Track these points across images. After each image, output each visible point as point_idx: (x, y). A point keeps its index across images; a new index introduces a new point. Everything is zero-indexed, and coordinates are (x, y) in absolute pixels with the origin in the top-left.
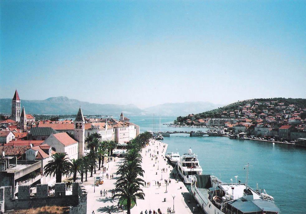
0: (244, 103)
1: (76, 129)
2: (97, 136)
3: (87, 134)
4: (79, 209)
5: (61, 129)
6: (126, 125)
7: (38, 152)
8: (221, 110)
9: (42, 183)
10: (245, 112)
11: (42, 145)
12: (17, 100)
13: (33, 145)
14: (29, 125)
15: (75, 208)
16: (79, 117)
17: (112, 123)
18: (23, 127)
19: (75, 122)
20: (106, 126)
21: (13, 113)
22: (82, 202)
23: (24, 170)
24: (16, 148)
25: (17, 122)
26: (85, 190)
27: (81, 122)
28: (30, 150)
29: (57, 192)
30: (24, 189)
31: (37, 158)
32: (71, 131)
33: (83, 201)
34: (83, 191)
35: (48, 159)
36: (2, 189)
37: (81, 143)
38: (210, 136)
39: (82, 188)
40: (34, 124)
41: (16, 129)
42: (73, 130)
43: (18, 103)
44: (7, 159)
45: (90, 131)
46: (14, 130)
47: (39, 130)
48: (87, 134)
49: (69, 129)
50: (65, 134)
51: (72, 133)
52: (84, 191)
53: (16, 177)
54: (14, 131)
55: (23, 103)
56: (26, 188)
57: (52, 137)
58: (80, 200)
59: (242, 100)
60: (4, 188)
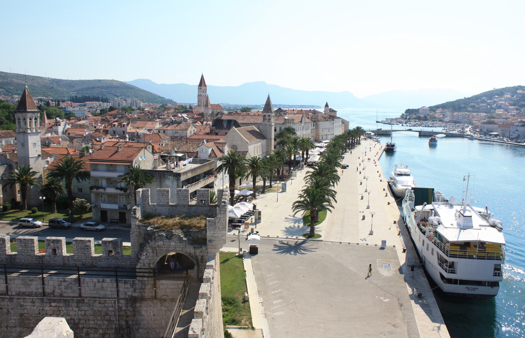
0: (501, 92)
4: (217, 222)
8: (467, 100)
10: (502, 104)
21: (199, 102)
22: (220, 213)
23: (192, 170)
24: (190, 143)
29: (200, 199)
30: (162, 193)
32: (260, 125)
33: (222, 212)
56: (165, 192)
58: (218, 211)
59: (500, 86)
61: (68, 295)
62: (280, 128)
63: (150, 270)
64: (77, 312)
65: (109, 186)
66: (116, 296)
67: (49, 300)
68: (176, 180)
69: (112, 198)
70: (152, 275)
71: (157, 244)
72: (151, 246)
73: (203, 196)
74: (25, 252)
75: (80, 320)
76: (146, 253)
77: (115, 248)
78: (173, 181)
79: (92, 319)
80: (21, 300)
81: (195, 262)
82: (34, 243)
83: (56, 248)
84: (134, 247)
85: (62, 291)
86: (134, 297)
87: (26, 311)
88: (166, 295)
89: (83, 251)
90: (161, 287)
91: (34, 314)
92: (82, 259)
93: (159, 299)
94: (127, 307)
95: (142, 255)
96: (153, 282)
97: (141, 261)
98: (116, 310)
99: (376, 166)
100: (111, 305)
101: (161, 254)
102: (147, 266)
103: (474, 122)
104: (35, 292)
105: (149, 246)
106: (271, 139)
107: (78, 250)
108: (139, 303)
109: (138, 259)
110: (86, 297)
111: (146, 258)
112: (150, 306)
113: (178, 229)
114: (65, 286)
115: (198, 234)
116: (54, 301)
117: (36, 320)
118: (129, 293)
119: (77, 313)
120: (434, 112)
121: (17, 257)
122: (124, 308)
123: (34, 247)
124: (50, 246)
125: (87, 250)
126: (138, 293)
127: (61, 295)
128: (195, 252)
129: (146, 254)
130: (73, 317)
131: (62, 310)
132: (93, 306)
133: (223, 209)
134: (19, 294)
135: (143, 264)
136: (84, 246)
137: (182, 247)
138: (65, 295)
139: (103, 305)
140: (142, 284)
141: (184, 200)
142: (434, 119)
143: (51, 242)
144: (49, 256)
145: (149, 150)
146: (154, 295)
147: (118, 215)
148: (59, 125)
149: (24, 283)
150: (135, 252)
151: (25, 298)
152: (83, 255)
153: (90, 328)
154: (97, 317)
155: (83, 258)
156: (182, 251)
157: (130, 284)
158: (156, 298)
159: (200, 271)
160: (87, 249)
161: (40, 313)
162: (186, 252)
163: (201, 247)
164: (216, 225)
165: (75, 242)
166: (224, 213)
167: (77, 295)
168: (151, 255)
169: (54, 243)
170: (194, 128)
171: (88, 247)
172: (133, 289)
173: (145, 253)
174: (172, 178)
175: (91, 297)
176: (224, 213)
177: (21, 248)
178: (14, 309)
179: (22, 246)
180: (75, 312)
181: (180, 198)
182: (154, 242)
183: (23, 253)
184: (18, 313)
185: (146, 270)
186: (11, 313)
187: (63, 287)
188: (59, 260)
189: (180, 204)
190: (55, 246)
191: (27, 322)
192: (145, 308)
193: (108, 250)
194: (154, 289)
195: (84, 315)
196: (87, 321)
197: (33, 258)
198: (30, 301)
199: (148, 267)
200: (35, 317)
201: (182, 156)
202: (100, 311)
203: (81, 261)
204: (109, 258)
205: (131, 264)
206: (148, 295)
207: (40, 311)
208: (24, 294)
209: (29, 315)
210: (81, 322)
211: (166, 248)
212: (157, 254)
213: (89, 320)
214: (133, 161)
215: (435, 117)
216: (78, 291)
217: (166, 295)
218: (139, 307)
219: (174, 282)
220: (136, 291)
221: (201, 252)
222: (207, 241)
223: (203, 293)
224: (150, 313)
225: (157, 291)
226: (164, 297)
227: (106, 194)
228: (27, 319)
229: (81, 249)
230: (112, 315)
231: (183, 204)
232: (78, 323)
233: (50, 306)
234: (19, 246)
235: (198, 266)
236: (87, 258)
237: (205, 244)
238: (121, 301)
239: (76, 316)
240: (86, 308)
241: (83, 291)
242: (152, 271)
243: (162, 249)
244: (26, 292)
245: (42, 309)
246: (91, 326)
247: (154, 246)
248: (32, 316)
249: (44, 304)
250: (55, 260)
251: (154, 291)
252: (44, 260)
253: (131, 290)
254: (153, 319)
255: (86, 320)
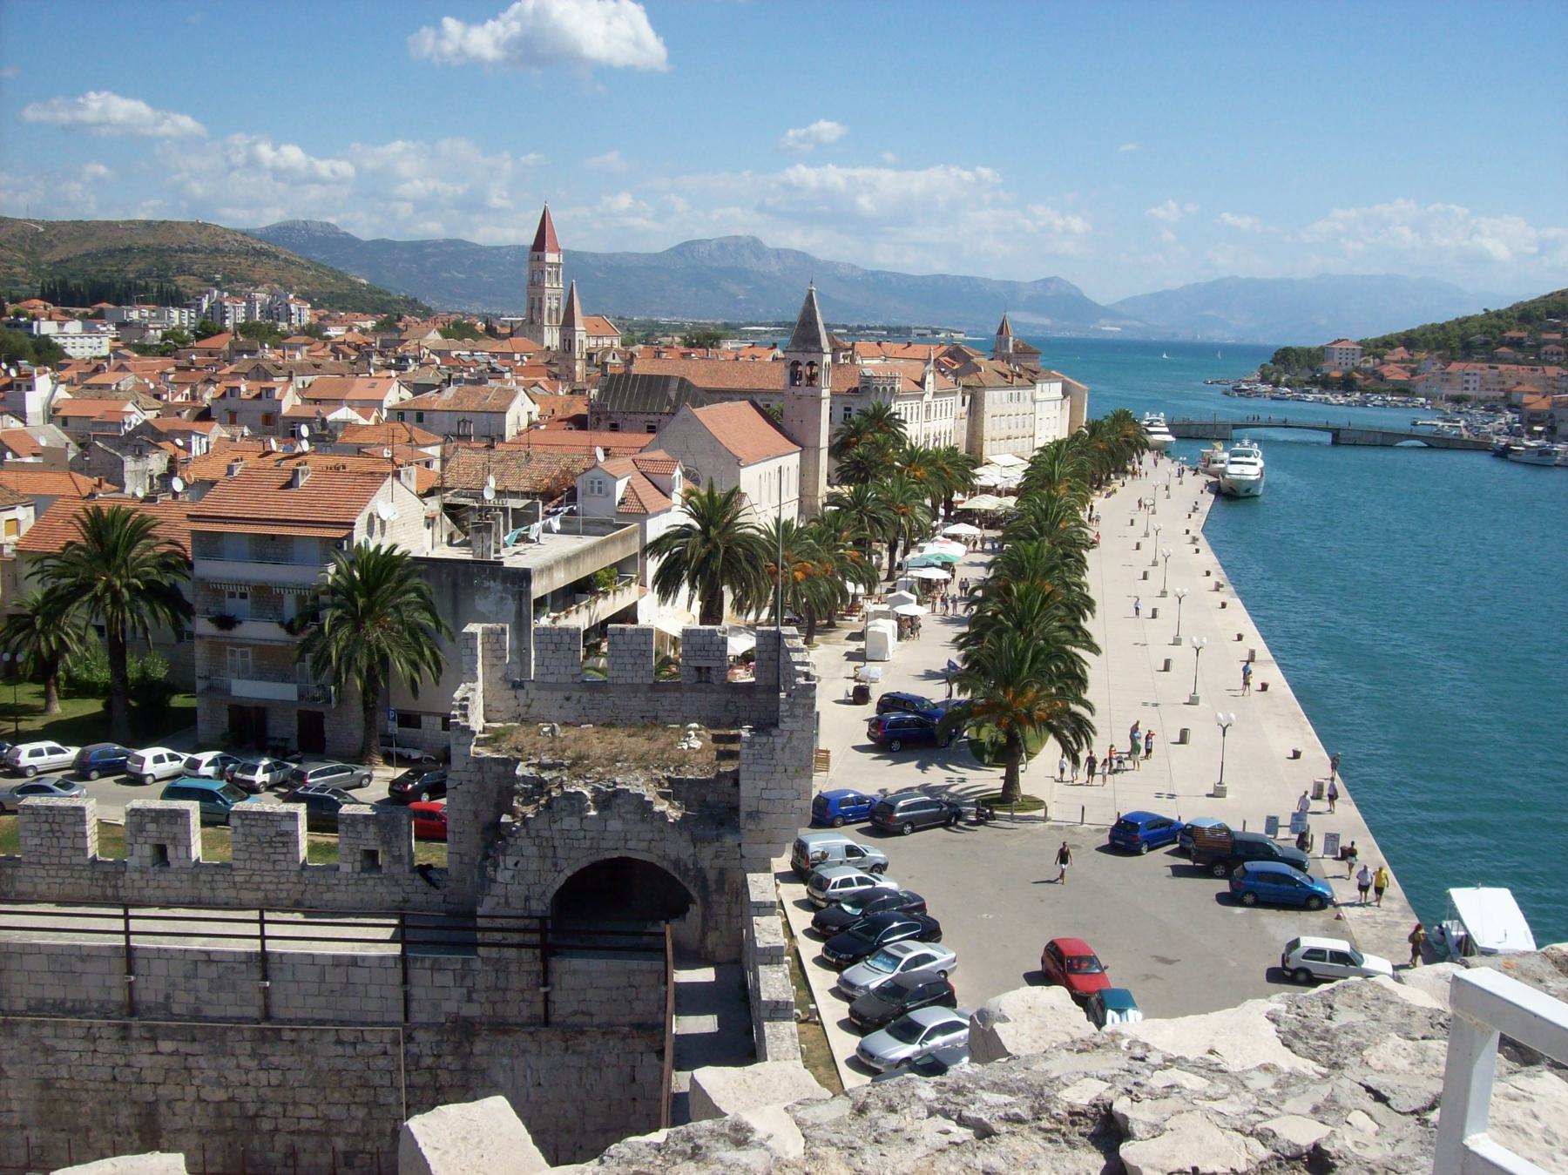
1: (794, 389)
2: (884, 422)
3: (842, 412)
4: (779, 747)
5: (730, 385)
6: (1020, 376)
7: (628, 483)
8: (1495, 321)
9: (644, 620)
11: (646, 455)
12: (552, 251)
13: (607, 452)
14: (597, 366)
15: (764, 739)
16: (805, 333)
17: (956, 367)
18: (572, 371)
19: (788, 355)
20: (929, 378)
21: (532, 308)
22: (793, 716)
23: (570, 560)
24: (539, 461)
25: (548, 348)
26: (807, 664)
27: (813, 357)
28: (594, 472)
29: (692, 663)
30: (556, 639)
31: (623, 509)
32: (771, 397)
33: (799, 711)
34: (798, 668)
35: (671, 517)
36: (473, 636)
37: (812, 452)
38: (1430, 447)
39: (796, 657)
40: (618, 360)
41: (543, 380)
42: (777, 393)
43: (551, 265)
44: (505, 510)
45: (852, 400)
46: (536, 384)
47: (633, 386)
48: (840, 413)
49: (758, 385)
50: (744, 407)
51: (776, 405)
52: (805, 669)
53: (539, 588)
54: (536, 389)
55: (577, 264)
56: (567, 639)
57: (685, 420)
58: (783, 707)
60: (479, 631)
61: (223, 1014)
62: (846, 409)
63: (527, 922)
64: (251, 1076)
65: (261, 616)
66: (401, 1018)
67: (151, 1029)
68: (513, 596)
69: (269, 663)
70: (536, 938)
71: (555, 827)
72: (533, 833)
73: (704, 653)
74: (50, 857)
75: (263, 1102)
76: (515, 859)
77: (386, 842)
78: (501, 598)
79: (308, 1099)
80: (48, 1031)
81: (694, 893)
82: (83, 821)
83: (167, 842)
84: (458, 836)
85: (197, 998)
86: (465, 1019)
87: (64, 1072)
88: (583, 1013)
89: (268, 854)
90: (568, 981)
91: (95, 1080)
92: (263, 882)
93: (558, 1024)
94: (439, 1056)
95: (502, 864)
96: (538, 966)
97: (497, 890)
98: (399, 1066)
99: (1197, 551)
100: (378, 1048)
101: (571, 862)
102: (517, 906)
103: (1526, 399)
104: (98, 1001)
105: (528, 832)
106: (818, 449)
107: (250, 849)
108: (484, 1040)
109: (487, 882)
110: (290, 1021)
111: (513, 877)
112: (525, 1052)
113: (629, 770)
114: (211, 981)
115: (703, 791)
116: (170, 1035)
117: (99, 1102)
118: (450, 1007)
119: (255, 1079)
120: (1377, 360)
121: (21, 873)
122: (428, 1061)
123: (84, 835)
124: (145, 834)
125: (285, 850)
126: (481, 1003)
127: (197, 1015)
128: (695, 855)
129: (516, 864)
130: (239, 1092)
131: (199, 1068)
132: (314, 1053)
133: (804, 701)
134: (38, 1008)
135: (502, 901)
136: (273, 834)
137: (650, 836)
138: (209, 1011)
139: (349, 1050)
140: (497, 971)
141: (636, 667)
142: (1379, 382)
143: (148, 820)
144: (142, 872)
145: (407, 484)
146: (539, 1009)
147: (295, 723)
148: (30, 388)
149: (57, 968)
150: (461, 855)
151: (64, 1024)
152: (269, 866)
153: (300, 1132)
154: (328, 1091)
155: (267, 879)
156: (649, 850)
157: (454, 970)
158: (547, 1023)
159: (711, 924)
160: (285, 844)
161: (115, 1079)
162: (664, 857)
163: (718, 838)
164: (776, 756)
165: (240, 817)
166: (805, 716)
167: (254, 1012)
168: (534, 867)
169: (162, 821)
170: (529, 405)
171: (285, 839)
172: (465, 990)
173: (510, 861)
174: (500, 588)
175: (305, 1022)
176: (805, 716)
177: (37, 841)
178: (21, 1062)
179: (39, 832)
180: (247, 1074)
181: (619, 661)
182: (547, 820)
183: (45, 860)
184: (36, 1075)
185: (513, 923)
186: (7, 1077)
187: (202, 984)
188: (178, 884)
189: (621, 681)
190: (164, 835)
191: (67, 1108)
192: (505, 1061)
193: (362, 847)
194: (542, 990)
195: (278, 1086)
196: (290, 1108)
197: (80, 878)
198: (80, 1033)
199: (520, 912)
200: (96, 1091)
201: (526, 507)
202: (340, 1071)
203: (259, 889)
204: (365, 879)
205: (444, 901)
206: (520, 1012)
207: (116, 1070)
208: (60, 1008)
209: (77, 1085)
210: (268, 1112)
211: (588, 843)
212: (555, 865)
213: (295, 1104)
214: (353, 524)
215: (1382, 378)
216: (261, 996)
217: (583, 1013)
218: (482, 1055)
219: (617, 964)
220: (475, 996)
221: (717, 856)
222: (742, 815)
223: (777, 1002)
224: (525, 1076)
225: (552, 997)
226: (578, 1019)
227: (249, 645)
228: (69, 1100)
229: (260, 843)
230: (383, 1086)
231: (629, 681)
232: (256, 1116)
233: (152, 1054)
234: (28, 834)
235: (707, 904)
236: (283, 880)
237: (736, 828)
238: (420, 1035)
239: (249, 1088)
240: (288, 1061)
241: (277, 998)
242: (535, 924)
243: (576, 844)
244: (63, 1002)
245: (122, 1062)
246: (305, 1124)
247: (546, 834)
248: (87, 1091)
249: (133, 1045)
250: (164, 884)
251: (540, 998)
252: (120, 883)
253: (458, 993)
254: (532, 1097)
255: (284, 1104)
